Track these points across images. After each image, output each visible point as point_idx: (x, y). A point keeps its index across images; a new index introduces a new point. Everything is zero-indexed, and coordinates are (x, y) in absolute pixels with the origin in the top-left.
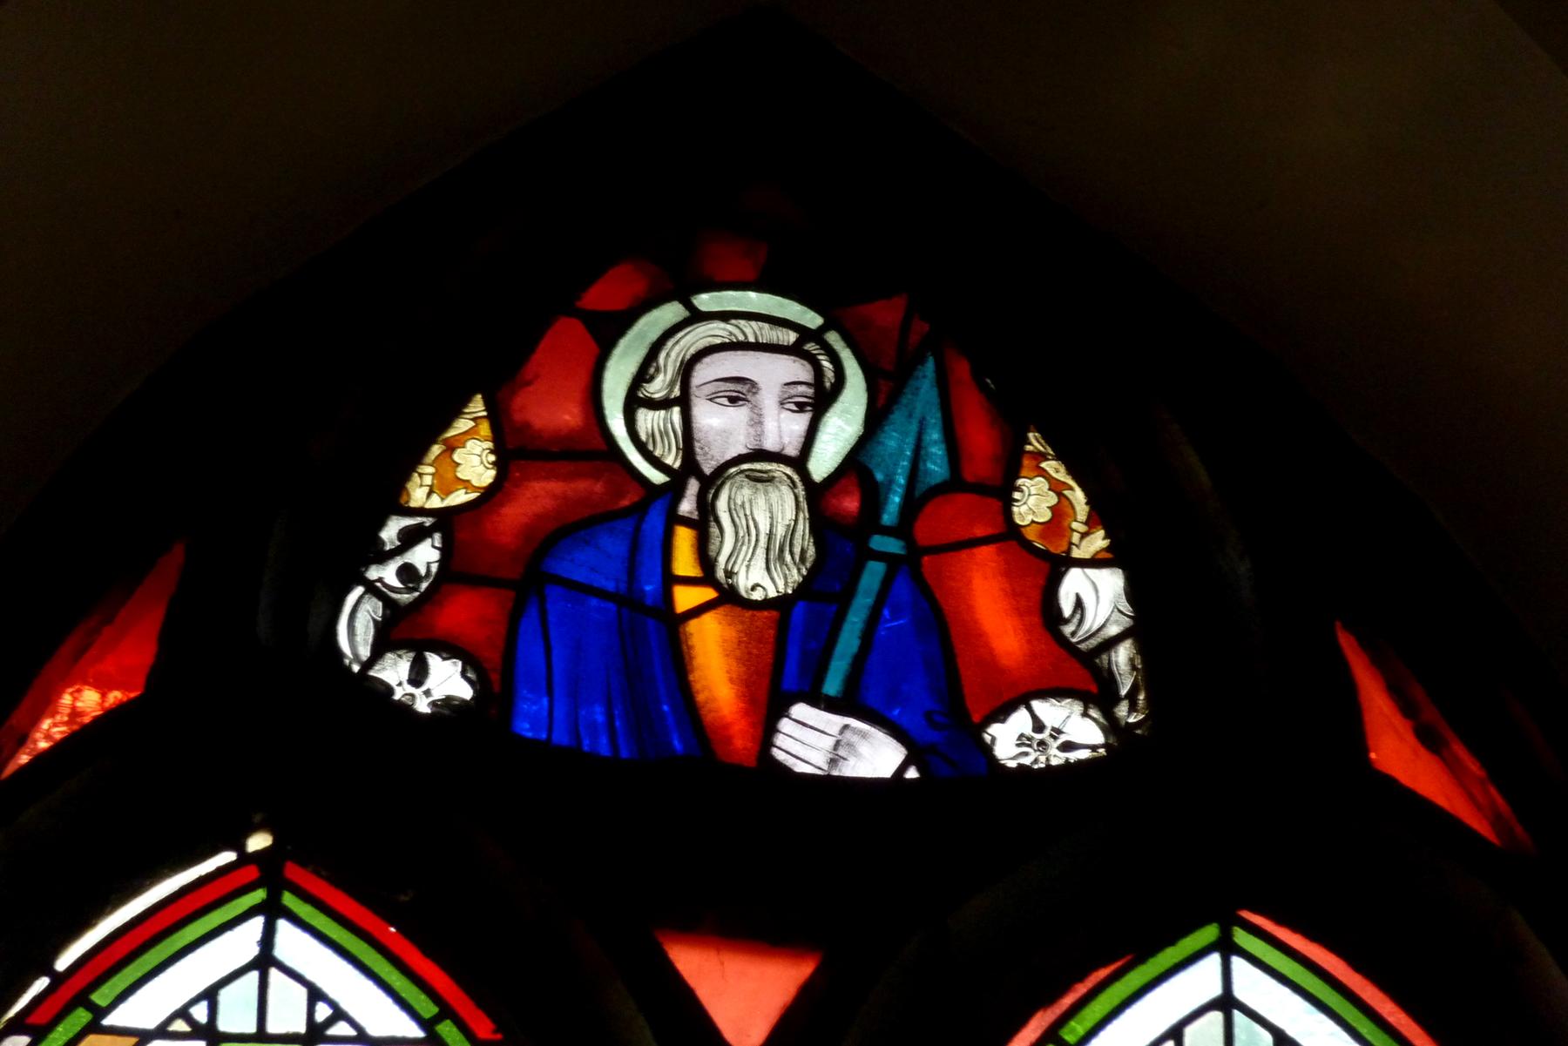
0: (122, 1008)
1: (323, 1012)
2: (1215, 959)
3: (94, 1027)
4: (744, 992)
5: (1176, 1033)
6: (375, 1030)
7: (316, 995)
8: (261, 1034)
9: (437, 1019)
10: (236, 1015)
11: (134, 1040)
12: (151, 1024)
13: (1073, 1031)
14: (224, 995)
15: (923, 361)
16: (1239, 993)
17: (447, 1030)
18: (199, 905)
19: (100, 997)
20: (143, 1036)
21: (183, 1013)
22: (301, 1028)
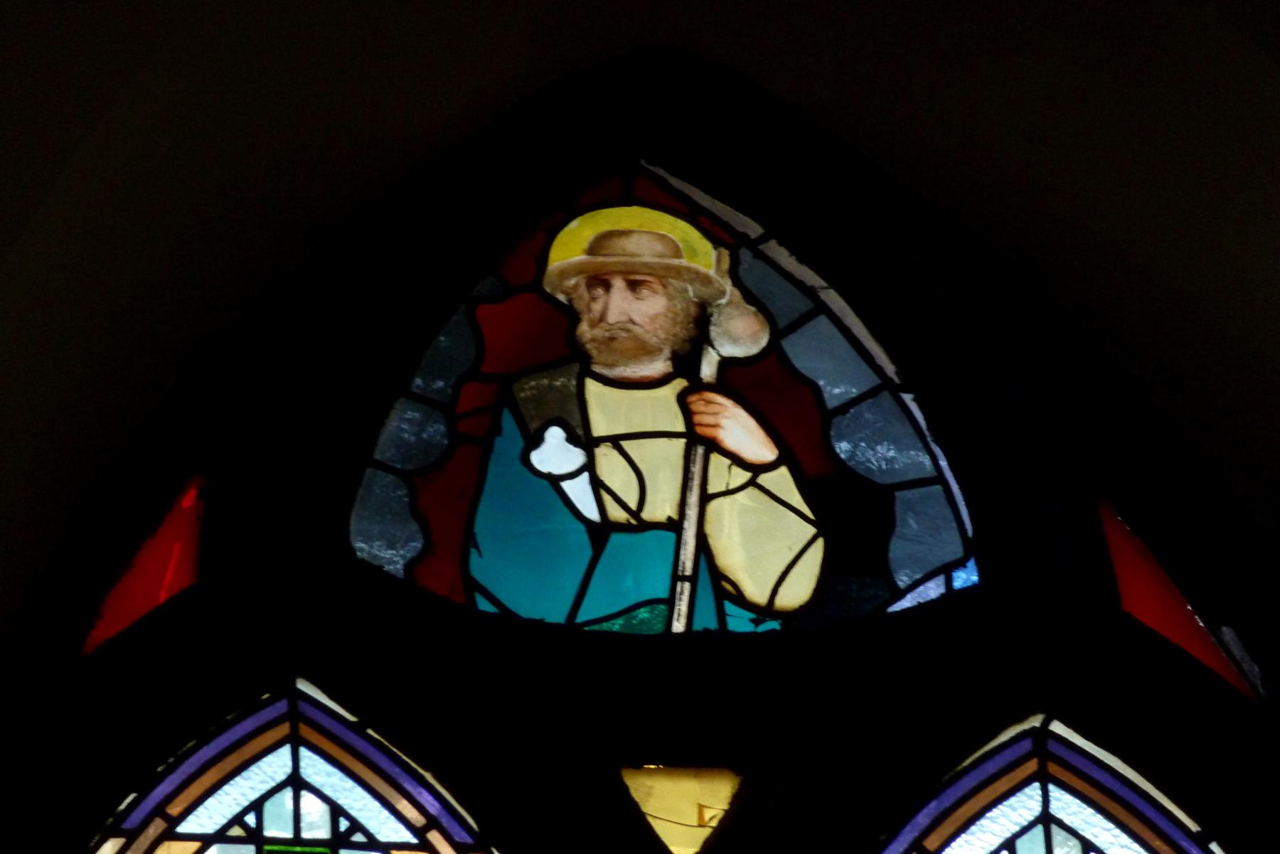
0: (191, 818)
1: (344, 824)
2: (286, 751)
3: (170, 835)
4: (683, 807)
5: (1010, 844)
6: (383, 837)
7: (337, 811)
8: (297, 840)
9: (427, 828)
10: (277, 827)
11: (195, 845)
12: (210, 828)
13: (931, 843)
14: (269, 807)
15: (497, 430)
16: (1055, 809)
17: (434, 837)
18: (1086, 762)
19: (174, 810)
20: (206, 841)
21: (238, 820)
22: (324, 833)
